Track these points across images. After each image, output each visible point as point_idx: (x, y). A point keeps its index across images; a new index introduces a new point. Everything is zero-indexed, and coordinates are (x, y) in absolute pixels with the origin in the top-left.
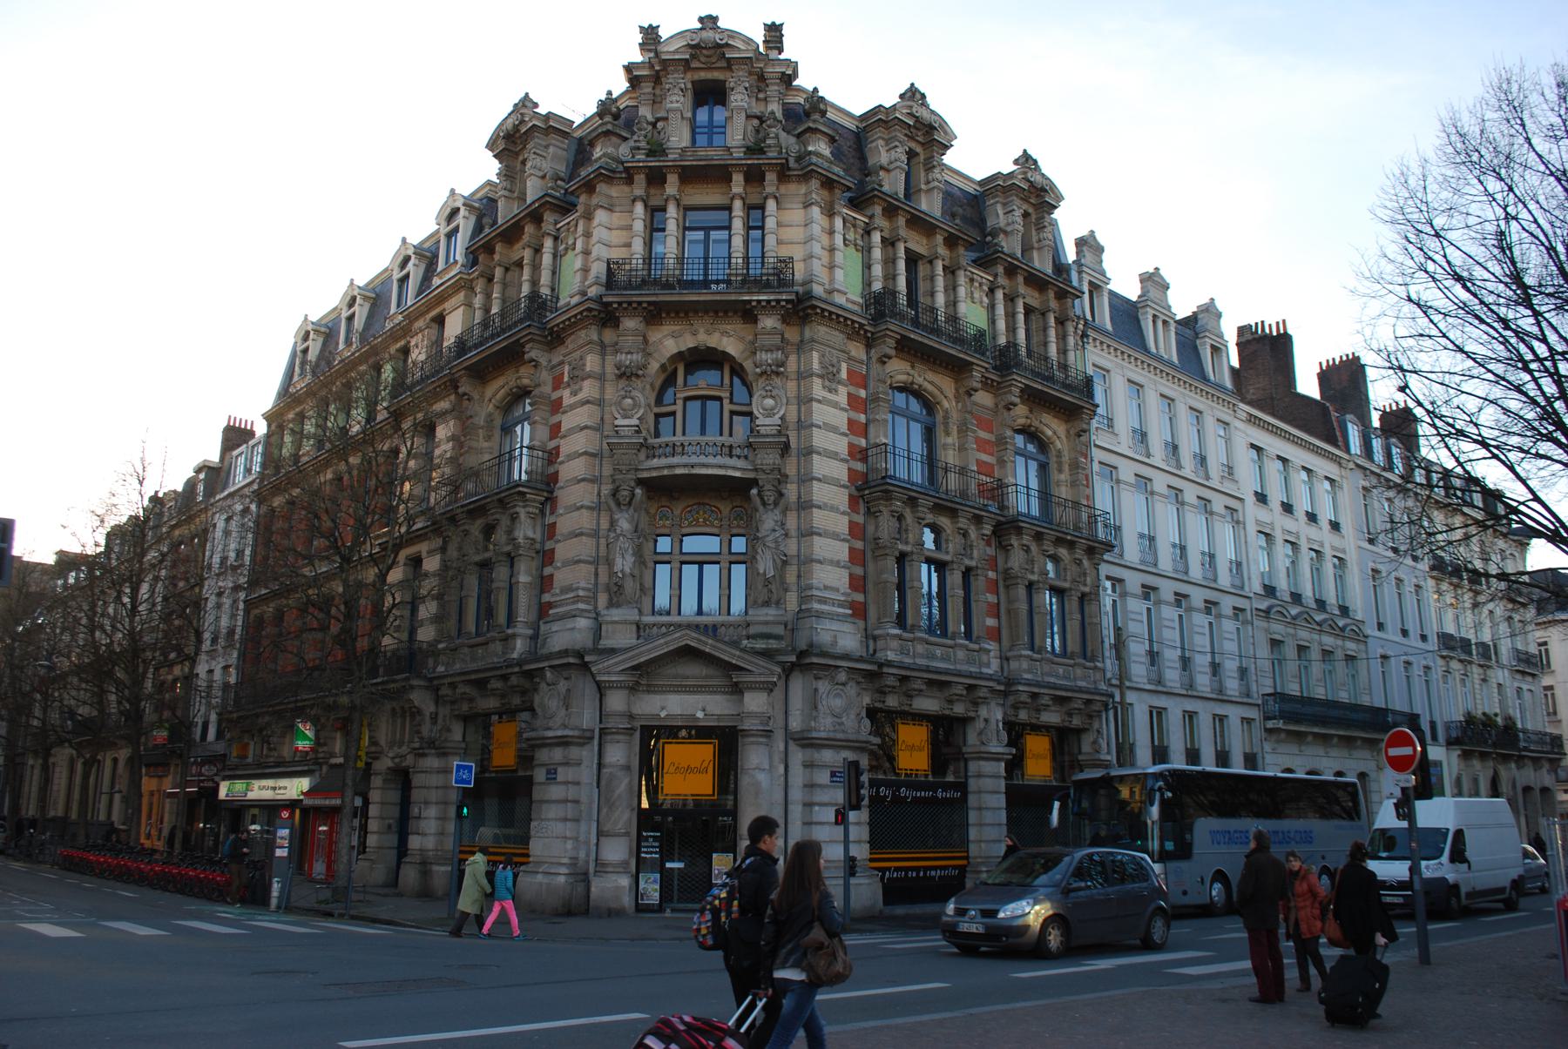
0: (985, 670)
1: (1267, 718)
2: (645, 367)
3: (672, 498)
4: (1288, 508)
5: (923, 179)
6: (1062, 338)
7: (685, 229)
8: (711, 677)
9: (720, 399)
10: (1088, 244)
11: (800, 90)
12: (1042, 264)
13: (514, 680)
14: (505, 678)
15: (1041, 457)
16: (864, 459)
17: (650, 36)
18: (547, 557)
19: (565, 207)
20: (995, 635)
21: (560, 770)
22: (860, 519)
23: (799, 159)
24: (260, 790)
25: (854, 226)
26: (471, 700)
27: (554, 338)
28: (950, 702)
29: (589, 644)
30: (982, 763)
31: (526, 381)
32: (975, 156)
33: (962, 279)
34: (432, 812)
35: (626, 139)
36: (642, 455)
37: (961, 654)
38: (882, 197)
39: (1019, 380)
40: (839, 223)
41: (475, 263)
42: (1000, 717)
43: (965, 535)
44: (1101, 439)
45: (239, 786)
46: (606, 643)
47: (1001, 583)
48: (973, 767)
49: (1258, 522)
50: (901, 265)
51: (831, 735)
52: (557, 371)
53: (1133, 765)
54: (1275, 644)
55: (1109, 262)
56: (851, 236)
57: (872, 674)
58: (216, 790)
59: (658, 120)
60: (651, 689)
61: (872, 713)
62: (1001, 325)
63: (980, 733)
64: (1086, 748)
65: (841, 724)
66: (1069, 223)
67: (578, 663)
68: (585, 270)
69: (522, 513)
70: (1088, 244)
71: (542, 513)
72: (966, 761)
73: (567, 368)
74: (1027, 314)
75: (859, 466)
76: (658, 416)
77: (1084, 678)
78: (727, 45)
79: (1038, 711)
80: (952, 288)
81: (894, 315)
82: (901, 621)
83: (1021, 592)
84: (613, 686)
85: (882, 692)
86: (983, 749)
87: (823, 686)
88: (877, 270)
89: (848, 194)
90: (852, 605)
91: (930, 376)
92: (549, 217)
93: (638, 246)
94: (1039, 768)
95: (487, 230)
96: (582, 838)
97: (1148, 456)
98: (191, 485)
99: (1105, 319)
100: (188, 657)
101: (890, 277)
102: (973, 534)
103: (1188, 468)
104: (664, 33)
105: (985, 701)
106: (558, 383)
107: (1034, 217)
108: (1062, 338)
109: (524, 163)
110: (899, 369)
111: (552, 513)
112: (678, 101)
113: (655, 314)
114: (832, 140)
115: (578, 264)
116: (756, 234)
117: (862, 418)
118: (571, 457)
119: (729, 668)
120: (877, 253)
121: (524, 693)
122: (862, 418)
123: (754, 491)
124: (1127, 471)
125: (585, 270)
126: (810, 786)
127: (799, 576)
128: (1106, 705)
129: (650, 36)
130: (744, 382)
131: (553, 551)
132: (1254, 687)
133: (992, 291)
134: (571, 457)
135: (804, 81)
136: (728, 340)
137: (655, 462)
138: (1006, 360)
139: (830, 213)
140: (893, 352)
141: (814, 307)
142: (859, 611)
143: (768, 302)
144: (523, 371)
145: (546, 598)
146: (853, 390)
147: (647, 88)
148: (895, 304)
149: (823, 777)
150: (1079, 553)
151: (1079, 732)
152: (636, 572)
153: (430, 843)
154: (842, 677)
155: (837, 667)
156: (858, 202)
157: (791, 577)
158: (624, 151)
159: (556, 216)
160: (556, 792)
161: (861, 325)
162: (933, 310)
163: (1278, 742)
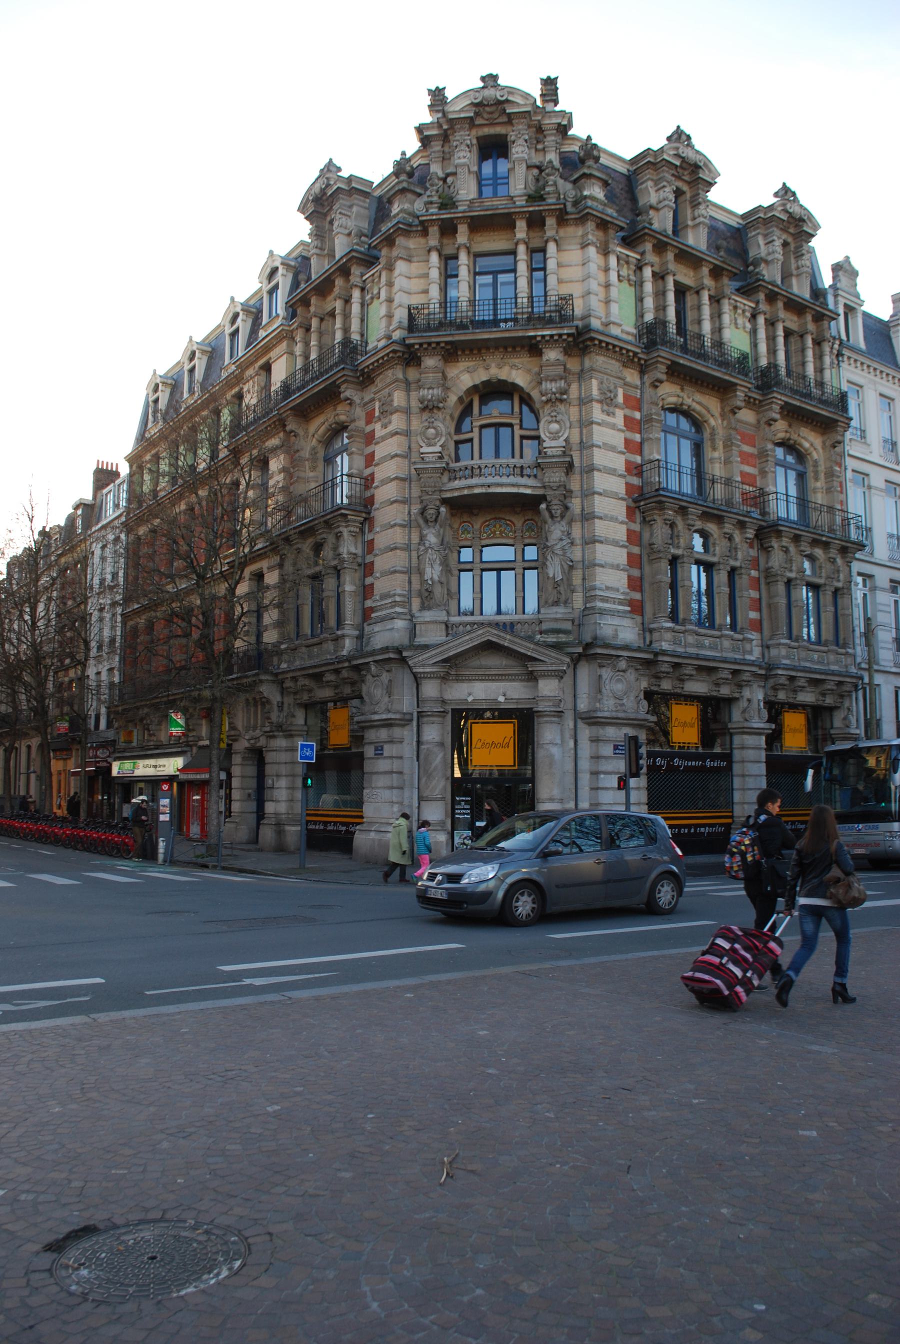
0: (748, 657)
2: (444, 400)
5: (689, 216)
6: (819, 357)
9: (511, 425)
10: (843, 269)
11: (575, 138)
12: (801, 289)
13: (345, 674)
15: (800, 468)
16: (640, 474)
17: (437, 97)
18: (368, 569)
19: (369, 261)
20: (757, 626)
22: (636, 527)
23: (575, 203)
24: (145, 768)
25: (627, 263)
26: (310, 691)
27: (366, 379)
28: (718, 685)
31: (343, 418)
32: (737, 192)
33: (726, 306)
34: (283, 783)
35: (419, 195)
39: (779, 398)
40: (613, 260)
41: (294, 315)
43: (730, 538)
44: (853, 448)
45: (128, 765)
47: (762, 581)
48: (737, 740)
50: (671, 297)
52: (369, 407)
55: (863, 286)
57: (649, 663)
58: (109, 769)
59: (448, 175)
61: (649, 695)
62: (763, 348)
63: (744, 711)
64: (838, 723)
66: (825, 251)
67: (397, 657)
68: (390, 316)
70: (843, 269)
71: (362, 531)
73: (377, 404)
75: (636, 481)
76: (457, 443)
77: (837, 662)
80: (717, 316)
83: (781, 588)
85: (657, 677)
86: (746, 724)
88: (649, 303)
89: (621, 234)
90: (631, 603)
91: (698, 397)
92: (356, 270)
94: (795, 740)
98: (71, 520)
99: (859, 338)
101: (661, 308)
102: (737, 537)
104: (450, 95)
106: (370, 418)
107: (792, 246)
108: (819, 357)
109: (331, 222)
110: (670, 392)
111: (370, 531)
113: (452, 352)
114: (605, 184)
115: (383, 311)
116: (539, 275)
117: (637, 437)
120: (648, 287)
121: (353, 684)
123: (543, 506)
125: (390, 316)
126: (596, 758)
127: (584, 579)
129: (437, 97)
130: (532, 410)
133: (754, 317)
134: (385, 482)
135: (578, 130)
136: (517, 372)
137: (457, 484)
138: (767, 380)
139: (605, 252)
140: (664, 377)
142: (637, 608)
143: (552, 336)
145: (369, 603)
146: (628, 412)
147: (437, 146)
148: (665, 333)
149: (608, 750)
150: (833, 553)
151: (831, 709)
152: (444, 580)
153: (282, 808)
154: (623, 664)
155: (619, 656)
157: (577, 579)
161: (635, 354)
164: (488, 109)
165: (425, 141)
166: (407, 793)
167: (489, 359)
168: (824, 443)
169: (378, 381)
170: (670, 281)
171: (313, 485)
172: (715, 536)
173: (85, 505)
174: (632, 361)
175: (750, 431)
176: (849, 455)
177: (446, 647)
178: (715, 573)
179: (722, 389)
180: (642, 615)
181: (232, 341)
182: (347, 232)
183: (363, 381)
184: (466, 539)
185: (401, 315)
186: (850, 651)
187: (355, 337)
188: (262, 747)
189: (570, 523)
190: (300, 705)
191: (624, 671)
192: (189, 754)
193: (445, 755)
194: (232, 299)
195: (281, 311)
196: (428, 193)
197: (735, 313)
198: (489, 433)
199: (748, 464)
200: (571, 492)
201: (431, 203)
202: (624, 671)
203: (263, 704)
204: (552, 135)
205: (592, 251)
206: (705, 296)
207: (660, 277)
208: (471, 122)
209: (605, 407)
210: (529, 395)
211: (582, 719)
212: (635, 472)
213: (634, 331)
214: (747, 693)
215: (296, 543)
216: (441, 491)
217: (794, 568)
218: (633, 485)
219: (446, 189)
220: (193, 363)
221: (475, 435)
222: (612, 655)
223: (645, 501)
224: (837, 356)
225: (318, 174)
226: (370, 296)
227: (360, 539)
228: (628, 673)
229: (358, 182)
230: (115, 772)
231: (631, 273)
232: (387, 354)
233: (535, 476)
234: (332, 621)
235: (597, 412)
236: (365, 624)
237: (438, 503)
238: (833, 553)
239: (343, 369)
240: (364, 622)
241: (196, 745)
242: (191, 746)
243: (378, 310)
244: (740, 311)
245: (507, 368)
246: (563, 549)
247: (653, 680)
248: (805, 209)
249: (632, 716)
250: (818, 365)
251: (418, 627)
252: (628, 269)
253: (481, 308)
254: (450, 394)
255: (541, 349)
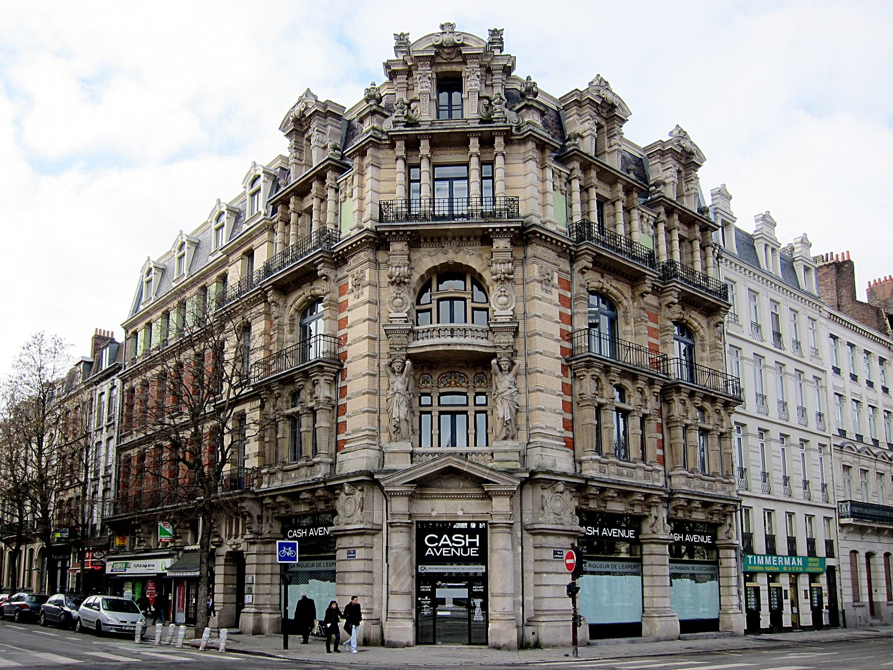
0: (656, 484)
1: (841, 517)
2: (409, 277)
3: (431, 368)
4: (854, 378)
5: (607, 145)
6: (705, 258)
7: (435, 180)
8: (467, 488)
9: (464, 299)
10: (722, 194)
11: (516, 79)
12: (691, 206)
13: (320, 493)
14: (313, 491)
15: (689, 341)
16: (571, 340)
17: (402, 42)
18: (340, 410)
19: (341, 168)
21: (357, 551)
22: (568, 381)
23: (518, 129)
24: (136, 568)
25: (560, 176)
26: (287, 507)
27: (339, 260)
28: (632, 505)
29: (376, 468)
30: (653, 545)
31: (318, 291)
32: (640, 132)
33: (635, 214)
35: (386, 117)
36: (411, 339)
37: (640, 473)
38: (578, 155)
39: (677, 285)
40: (549, 173)
41: (274, 211)
42: (665, 516)
43: (642, 392)
44: (729, 328)
45: (120, 565)
46: (387, 466)
47: (665, 426)
48: (646, 549)
49: (835, 387)
50: (594, 205)
51: (554, 527)
52: (343, 282)
53: (122, 595)
54: (847, 468)
55: (735, 207)
56: (557, 183)
57: (580, 488)
59: (412, 101)
60: (422, 497)
61: (579, 512)
62: (663, 248)
63: (652, 526)
65: (561, 519)
66: (707, 180)
67: (369, 481)
68: (361, 211)
69: (322, 380)
70: (722, 194)
71: (335, 380)
72: (641, 544)
73: (350, 280)
74: (680, 242)
75: (568, 345)
76: (418, 311)
77: (724, 489)
78: (463, 45)
79: (691, 511)
80: (628, 222)
81: (591, 239)
82: (598, 450)
83: (680, 431)
84: (394, 494)
85: (587, 498)
86: (654, 536)
87: (547, 494)
88: (577, 208)
89: (554, 155)
90: (565, 439)
91: (614, 283)
92: (330, 174)
93: (400, 192)
95: (282, 189)
96: (375, 596)
97: (763, 341)
98: (72, 375)
99: (732, 246)
100: (80, 483)
101: (586, 213)
102: (647, 392)
103: (789, 349)
104: (412, 40)
105: (656, 504)
106: (343, 291)
107: (683, 174)
108: (705, 258)
109: (309, 140)
110: (594, 279)
111: (343, 380)
112: (424, 85)
113: (415, 240)
114: (542, 114)
115: (356, 207)
116: (487, 183)
117: (569, 312)
118: (356, 341)
119: (480, 482)
120: (576, 196)
121: (327, 501)
122: (569, 312)
123: (494, 361)
124: (748, 351)
125: (361, 211)
127: (527, 420)
128: (736, 508)
129: (402, 42)
130: (481, 289)
131: (345, 405)
132: (831, 497)
133: (655, 225)
134: (356, 341)
135: (519, 72)
136: (470, 257)
137: (421, 343)
138: (668, 272)
139: (543, 167)
140: (590, 265)
141: (535, 232)
142: (570, 444)
143: (501, 229)
144: (316, 284)
145: (341, 437)
146: (563, 292)
147: (401, 79)
148: (590, 232)
150: (719, 406)
152: (408, 418)
154: (561, 487)
155: (557, 481)
156: (563, 159)
157: (522, 421)
158: (387, 125)
159: (336, 175)
160: (355, 565)
161: (568, 246)
162: (615, 237)
163: (848, 533)
164: (446, 50)
165: (393, 75)
166: (376, 588)
167: (447, 246)
168: (709, 323)
169: (351, 261)
170: (593, 192)
171: (290, 344)
172: (630, 390)
173: (85, 362)
174: (565, 251)
175: (653, 311)
176: (728, 333)
177: (413, 471)
178: (629, 418)
179: (634, 279)
180: (574, 450)
181: (180, 264)
182: (322, 146)
183: (337, 263)
184: (426, 387)
185: (371, 211)
186: (732, 480)
187: (330, 227)
188: (243, 551)
189: (516, 375)
190: (278, 518)
191: (561, 493)
192: (176, 557)
193: (411, 558)
194: (219, 201)
195: (262, 210)
196: (395, 114)
197: (642, 221)
198: (445, 305)
199: (652, 336)
200: (517, 351)
201: (399, 122)
202: (561, 493)
203: (244, 518)
204: (499, 74)
205: (532, 165)
206: (620, 206)
207: (584, 189)
208: (432, 61)
209: (544, 287)
210: (480, 275)
211: (527, 530)
212: (567, 338)
213: (566, 230)
214: (654, 512)
215: (316, 376)
216: (407, 348)
217: (689, 416)
218: (565, 348)
219: (410, 112)
220: (182, 252)
221: (434, 306)
222: (553, 480)
223: (573, 363)
224: (717, 259)
225: (296, 101)
226: (343, 195)
227: (333, 387)
228: (564, 496)
229: (332, 107)
230: (108, 571)
231: (563, 184)
232: (360, 240)
233: (487, 338)
234: (307, 449)
235: (536, 289)
236: (338, 454)
237: (404, 358)
238: (719, 406)
239: (321, 251)
240: (336, 452)
241: (182, 550)
242: (178, 550)
243: (350, 207)
244: (645, 220)
245: (461, 253)
246: (511, 395)
247: (583, 500)
248: (695, 145)
249: (568, 528)
250: (704, 265)
251: (386, 456)
252: (560, 181)
253: (441, 205)
254: (413, 273)
255: (492, 239)
